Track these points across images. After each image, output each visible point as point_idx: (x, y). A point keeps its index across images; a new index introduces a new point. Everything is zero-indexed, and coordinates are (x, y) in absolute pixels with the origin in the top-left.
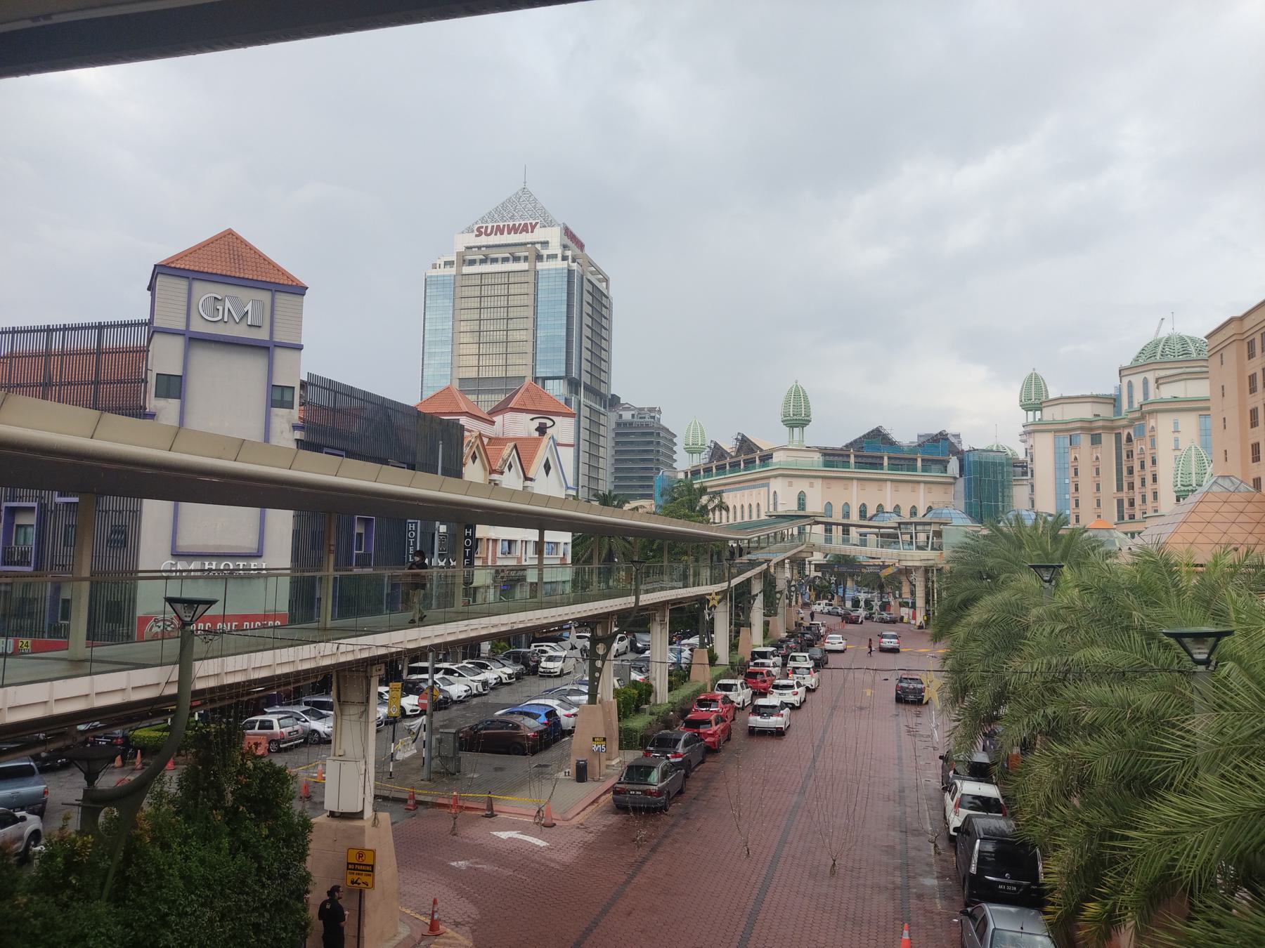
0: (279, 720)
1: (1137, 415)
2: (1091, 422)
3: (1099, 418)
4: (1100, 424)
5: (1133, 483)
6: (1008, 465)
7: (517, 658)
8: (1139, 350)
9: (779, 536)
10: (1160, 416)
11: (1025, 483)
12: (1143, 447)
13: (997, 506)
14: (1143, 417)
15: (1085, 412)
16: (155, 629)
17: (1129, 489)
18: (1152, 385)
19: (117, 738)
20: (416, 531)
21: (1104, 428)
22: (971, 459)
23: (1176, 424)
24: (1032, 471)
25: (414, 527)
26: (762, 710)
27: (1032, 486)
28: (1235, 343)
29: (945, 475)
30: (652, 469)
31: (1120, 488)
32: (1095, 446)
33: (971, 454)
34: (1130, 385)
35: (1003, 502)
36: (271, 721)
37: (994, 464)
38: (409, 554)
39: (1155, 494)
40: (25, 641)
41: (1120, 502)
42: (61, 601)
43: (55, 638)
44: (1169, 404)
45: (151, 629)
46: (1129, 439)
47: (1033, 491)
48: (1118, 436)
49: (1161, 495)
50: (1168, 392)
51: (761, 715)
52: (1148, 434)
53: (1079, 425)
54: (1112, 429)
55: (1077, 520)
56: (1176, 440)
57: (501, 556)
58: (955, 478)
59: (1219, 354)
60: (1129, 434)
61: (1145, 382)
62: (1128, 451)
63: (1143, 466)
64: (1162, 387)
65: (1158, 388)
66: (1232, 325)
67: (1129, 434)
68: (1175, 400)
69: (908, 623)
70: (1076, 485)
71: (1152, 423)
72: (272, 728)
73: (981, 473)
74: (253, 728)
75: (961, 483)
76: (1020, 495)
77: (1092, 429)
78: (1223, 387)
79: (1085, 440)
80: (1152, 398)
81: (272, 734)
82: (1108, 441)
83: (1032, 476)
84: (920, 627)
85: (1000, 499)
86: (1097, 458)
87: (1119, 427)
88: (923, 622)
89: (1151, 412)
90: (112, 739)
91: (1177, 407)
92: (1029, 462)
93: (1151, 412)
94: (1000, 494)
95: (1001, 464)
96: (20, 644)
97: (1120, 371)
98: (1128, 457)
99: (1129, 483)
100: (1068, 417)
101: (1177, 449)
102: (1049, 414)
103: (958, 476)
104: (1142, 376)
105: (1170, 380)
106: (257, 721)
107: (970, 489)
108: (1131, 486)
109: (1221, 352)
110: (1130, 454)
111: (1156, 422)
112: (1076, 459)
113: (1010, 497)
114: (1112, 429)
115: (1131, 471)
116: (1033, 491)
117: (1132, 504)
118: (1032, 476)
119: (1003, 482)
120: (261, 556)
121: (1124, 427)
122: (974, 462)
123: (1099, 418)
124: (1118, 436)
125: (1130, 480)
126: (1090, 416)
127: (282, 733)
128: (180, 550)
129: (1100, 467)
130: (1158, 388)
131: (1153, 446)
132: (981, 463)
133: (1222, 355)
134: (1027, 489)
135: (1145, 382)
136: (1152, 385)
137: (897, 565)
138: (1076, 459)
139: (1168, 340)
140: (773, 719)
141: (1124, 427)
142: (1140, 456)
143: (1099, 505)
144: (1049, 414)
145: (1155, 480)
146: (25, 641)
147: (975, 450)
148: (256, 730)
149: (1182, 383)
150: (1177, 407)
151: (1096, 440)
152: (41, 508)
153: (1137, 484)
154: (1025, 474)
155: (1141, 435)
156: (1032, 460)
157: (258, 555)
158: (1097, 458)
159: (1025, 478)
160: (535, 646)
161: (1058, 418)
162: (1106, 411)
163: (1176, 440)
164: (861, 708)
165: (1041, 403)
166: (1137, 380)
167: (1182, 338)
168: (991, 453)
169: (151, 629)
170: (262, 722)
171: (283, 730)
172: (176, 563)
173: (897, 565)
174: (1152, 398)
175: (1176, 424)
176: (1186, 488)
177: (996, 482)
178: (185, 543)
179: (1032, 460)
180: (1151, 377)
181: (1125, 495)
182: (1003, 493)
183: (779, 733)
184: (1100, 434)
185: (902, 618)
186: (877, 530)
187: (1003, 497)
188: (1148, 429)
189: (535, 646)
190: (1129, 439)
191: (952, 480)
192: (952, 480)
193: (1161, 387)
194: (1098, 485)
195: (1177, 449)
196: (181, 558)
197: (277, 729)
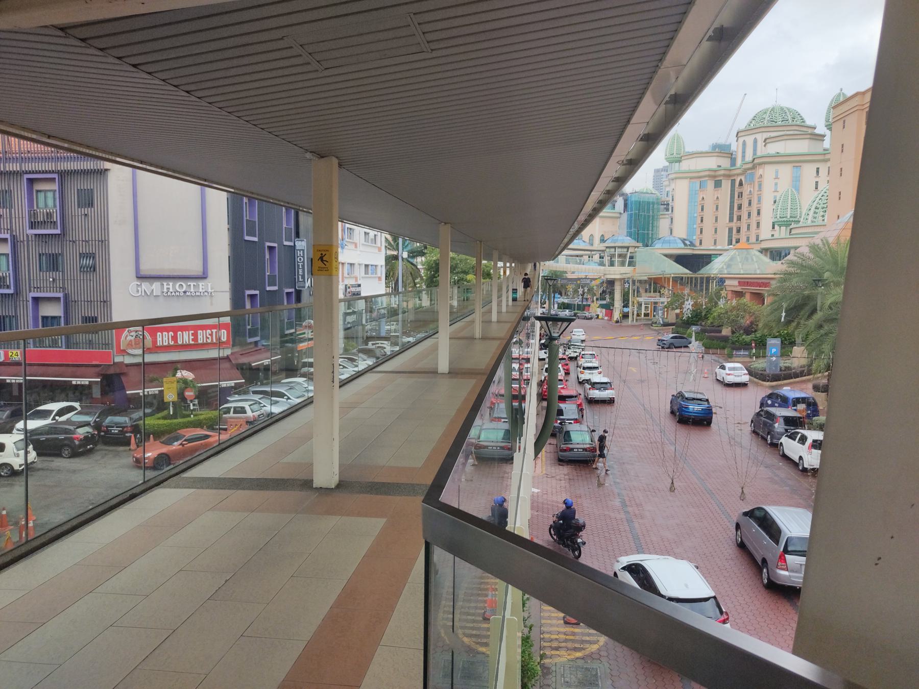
0: (250, 406)
1: (750, 166)
2: (715, 171)
3: (720, 168)
4: (722, 172)
5: (741, 216)
6: (658, 203)
7: (369, 353)
8: (752, 117)
9: (606, 260)
10: (767, 167)
11: (667, 216)
12: (752, 190)
13: (648, 234)
14: (754, 167)
15: (711, 163)
16: (129, 338)
17: (737, 220)
18: (760, 143)
19: (127, 427)
20: (303, 257)
21: (724, 175)
22: (633, 199)
23: (777, 172)
24: (672, 208)
25: (301, 253)
26: (598, 386)
27: (672, 219)
28: (857, 112)
29: (614, 211)
30: (34, 213)
31: (731, 220)
32: (716, 189)
33: (633, 195)
34: (744, 143)
35: (652, 231)
36: (243, 408)
37: (649, 203)
38: (298, 275)
39: (758, 224)
40: (14, 352)
41: (730, 230)
42: (40, 318)
43: (53, 347)
44: (771, 158)
45: (126, 338)
46: (741, 184)
47: (672, 222)
48: (733, 182)
49: (762, 225)
50: (773, 149)
51: (599, 389)
52: (756, 180)
53: (707, 173)
54: (729, 176)
55: (701, 243)
56: (776, 184)
57: (347, 276)
58: (620, 213)
59: (842, 121)
60: (741, 180)
61: (755, 141)
62: (739, 193)
63: (750, 204)
64: (768, 145)
65: (765, 146)
66: (856, 99)
67: (741, 180)
68: (778, 155)
69: (602, 319)
70: (702, 218)
71: (760, 171)
72: (245, 412)
73: (639, 210)
74: (229, 412)
75: (625, 217)
76: (663, 225)
77: (715, 177)
78: (843, 145)
79: (710, 184)
80: (759, 154)
81: (246, 418)
82: (726, 185)
83: (672, 211)
84: (617, 322)
85: (651, 229)
86: (718, 198)
87: (734, 175)
88: (619, 318)
89: (760, 164)
90: (123, 427)
91: (778, 160)
92: (671, 201)
93: (760, 164)
94: (651, 225)
95: (653, 203)
96: (10, 354)
97: (738, 133)
98: (739, 197)
99: (738, 216)
100: (699, 168)
101: (776, 191)
102: (686, 165)
103: (622, 212)
104: (753, 137)
105: (774, 140)
106: (231, 407)
107: (631, 221)
108: (739, 218)
109: (843, 119)
110: (741, 195)
111: (764, 171)
112: (703, 198)
113: (657, 227)
114: (729, 176)
115: (740, 207)
116: (672, 222)
117: (739, 231)
118: (672, 211)
119: (653, 216)
120: (205, 278)
121: (738, 175)
122: (635, 201)
123: (720, 168)
124: (733, 182)
125: (739, 214)
126: (714, 167)
127: (254, 416)
128: (142, 273)
129: (719, 205)
130: (765, 146)
131: (760, 189)
132: (640, 202)
133: (844, 121)
134: (669, 221)
135: (755, 141)
136: (760, 143)
137: (602, 278)
138: (703, 198)
139: (773, 109)
140: (607, 392)
141: (738, 175)
142: (749, 196)
143: (716, 232)
144: (686, 165)
145: (759, 213)
146: (14, 352)
147: (636, 192)
148: (231, 414)
149: (783, 142)
150: (778, 160)
151: (718, 184)
152: (14, 239)
153: (745, 216)
154: (667, 210)
155: (752, 182)
156: (673, 200)
157: (204, 277)
158: (718, 198)
159: (667, 213)
160: (373, 344)
161: (693, 168)
162: (725, 163)
163: (776, 184)
164: (642, 381)
165: (681, 158)
166: (749, 140)
167: (782, 109)
168: (647, 195)
169: (126, 338)
170: (235, 408)
171: (254, 414)
172: (141, 285)
173: (602, 278)
174: (759, 154)
175: (777, 172)
176: (783, 219)
177: (649, 216)
178: (147, 267)
179: (673, 200)
180: (760, 137)
181: (734, 225)
182: (652, 224)
183: (611, 401)
184: (721, 180)
185: (598, 316)
186: (590, 252)
187: (653, 227)
188: (757, 176)
189: (373, 344)
190: (741, 184)
191: (618, 215)
192: (618, 215)
193: (768, 145)
194: (717, 218)
195: (776, 191)
196: (145, 280)
197: (249, 414)
